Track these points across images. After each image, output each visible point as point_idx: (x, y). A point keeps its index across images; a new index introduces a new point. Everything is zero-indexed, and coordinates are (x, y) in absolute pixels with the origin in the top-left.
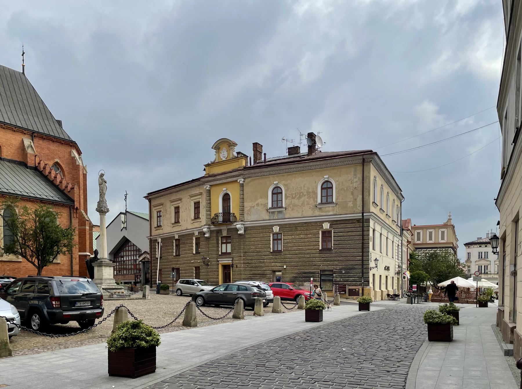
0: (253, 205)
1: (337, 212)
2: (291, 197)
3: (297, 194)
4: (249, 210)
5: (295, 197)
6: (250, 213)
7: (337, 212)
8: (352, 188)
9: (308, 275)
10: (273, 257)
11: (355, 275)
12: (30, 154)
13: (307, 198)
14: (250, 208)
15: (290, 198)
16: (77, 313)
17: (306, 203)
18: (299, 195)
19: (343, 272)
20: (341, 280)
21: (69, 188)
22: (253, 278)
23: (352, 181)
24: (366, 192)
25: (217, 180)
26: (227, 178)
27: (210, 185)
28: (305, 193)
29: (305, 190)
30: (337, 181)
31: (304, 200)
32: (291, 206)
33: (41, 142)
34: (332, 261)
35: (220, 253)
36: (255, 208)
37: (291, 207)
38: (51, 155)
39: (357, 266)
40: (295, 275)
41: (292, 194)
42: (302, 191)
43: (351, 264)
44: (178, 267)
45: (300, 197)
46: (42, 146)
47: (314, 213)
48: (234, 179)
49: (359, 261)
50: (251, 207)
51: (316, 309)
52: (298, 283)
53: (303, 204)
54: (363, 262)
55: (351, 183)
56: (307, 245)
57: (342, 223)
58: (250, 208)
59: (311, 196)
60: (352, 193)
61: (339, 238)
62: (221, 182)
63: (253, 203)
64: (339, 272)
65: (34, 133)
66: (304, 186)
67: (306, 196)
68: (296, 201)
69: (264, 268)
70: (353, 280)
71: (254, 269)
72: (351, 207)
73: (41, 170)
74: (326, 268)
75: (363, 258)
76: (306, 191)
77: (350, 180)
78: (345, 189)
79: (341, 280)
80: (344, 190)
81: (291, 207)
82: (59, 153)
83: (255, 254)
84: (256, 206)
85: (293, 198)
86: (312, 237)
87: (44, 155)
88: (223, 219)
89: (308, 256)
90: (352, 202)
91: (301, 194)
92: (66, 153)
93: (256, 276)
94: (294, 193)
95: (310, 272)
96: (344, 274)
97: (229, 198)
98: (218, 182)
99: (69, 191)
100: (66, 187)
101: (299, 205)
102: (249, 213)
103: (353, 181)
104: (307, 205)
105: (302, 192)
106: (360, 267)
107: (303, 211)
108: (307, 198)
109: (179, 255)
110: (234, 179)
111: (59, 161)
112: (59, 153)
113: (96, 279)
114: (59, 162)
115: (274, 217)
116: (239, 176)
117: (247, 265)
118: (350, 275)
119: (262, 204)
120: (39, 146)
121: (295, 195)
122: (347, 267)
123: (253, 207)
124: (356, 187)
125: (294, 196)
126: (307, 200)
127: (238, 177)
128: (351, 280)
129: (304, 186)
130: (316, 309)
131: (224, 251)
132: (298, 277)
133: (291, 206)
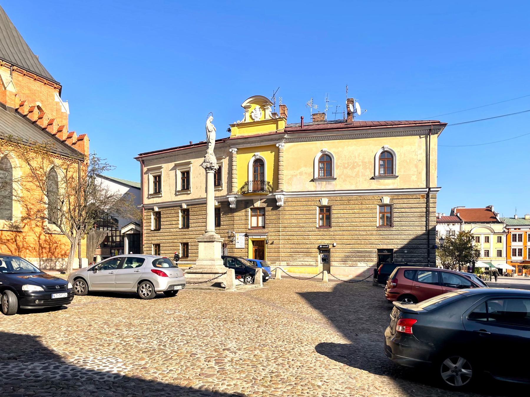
0: (295, 174)
1: (398, 185)
2: (343, 166)
3: (350, 164)
4: (291, 179)
5: (348, 167)
6: (292, 182)
7: (398, 185)
8: (416, 160)
9: (363, 254)
10: (321, 233)
11: (419, 256)
12: (10, 92)
13: (363, 169)
14: (291, 176)
15: (341, 168)
16: (58, 294)
17: (360, 174)
18: (352, 165)
19: (406, 252)
20: (403, 260)
21: (74, 139)
22: (294, 256)
23: (415, 153)
24: (432, 165)
25: (249, 143)
26: (262, 141)
27: (237, 149)
28: (360, 163)
29: (360, 159)
30: (399, 152)
31: (359, 171)
32: (343, 176)
33: (21, 78)
34: (392, 239)
35: (249, 227)
36: (298, 177)
37: (342, 178)
38: (31, 96)
39: (421, 245)
40: (348, 254)
41: (344, 163)
42: (357, 160)
43: (415, 243)
44: (158, 243)
45: (353, 168)
46: (22, 84)
47: (371, 186)
48: (272, 143)
49: (423, 239)
50: (293, 176)
51: (18, 269)
52: (351, 263)
53: (357, 175)
54: (428, 242)
55: (415, 155)
56: (362, 221)
57: (403, 198)
58: (291, 176)
59: (368, 167)
60: (416, 166)
61: (311, 216)
62: (253, 145)
63: (295, 171)
64: (401, 252)
65: (14, 65)
66: (359, 156)
67: (361, 166)
68: (348, 171)
69: (309, 246)
70: (417, 260)
71: (296, 246)
72: (415, 180)
73: (25, 114)
74: (385, 247)
75: (428, 237)
76: (361, 161)
77: (414, 151)
78: (408, 161)
79: (403, 260)
80: (406, 161)
81: (342, 178)
82: (41, 95)
83: (297, 229)
84: (299, 175)
85: (345, 168)
86: (369, 212)
87: (24, 96)
88: (254, 187)
89: (364, 233)
90: (415, 176)
91: (355, 164)
92: (49, 97)
93: (299, 254)
94: (347, 162)
95: (366, 251)
96: (407, 254)
97: (263, 164)
98: (249, 146)
99: (74, 142)
100: (69, 137)
101: (352, 176)
102: (290, 182)
103: (417, 153)
104: (362, 176)
105: (356, 162)
106: (426, 246)
107: (357, 183)
108: (363, 169)
109: (188, 227)
110: (272, 143)
111: (40, 105)
112: (41, 95)
113: (203, 260)
114: (40, 106)
115: (321, 187)
116: (279, 140)
117: (287, 242)
118: (413, 255)
119: (306, 173)
120: (18, 84)
121: (348, 165)
122: (410, 246)
123: (296, 176)
124: (421, 159)
125: (346, 165)
126: (362, 170)
127: (277, 140)
128: (414, 260)
129: (359, 156)
130: (18, 269)
131: (254, 225)
132: (351, 256)
133: (343, 176)
